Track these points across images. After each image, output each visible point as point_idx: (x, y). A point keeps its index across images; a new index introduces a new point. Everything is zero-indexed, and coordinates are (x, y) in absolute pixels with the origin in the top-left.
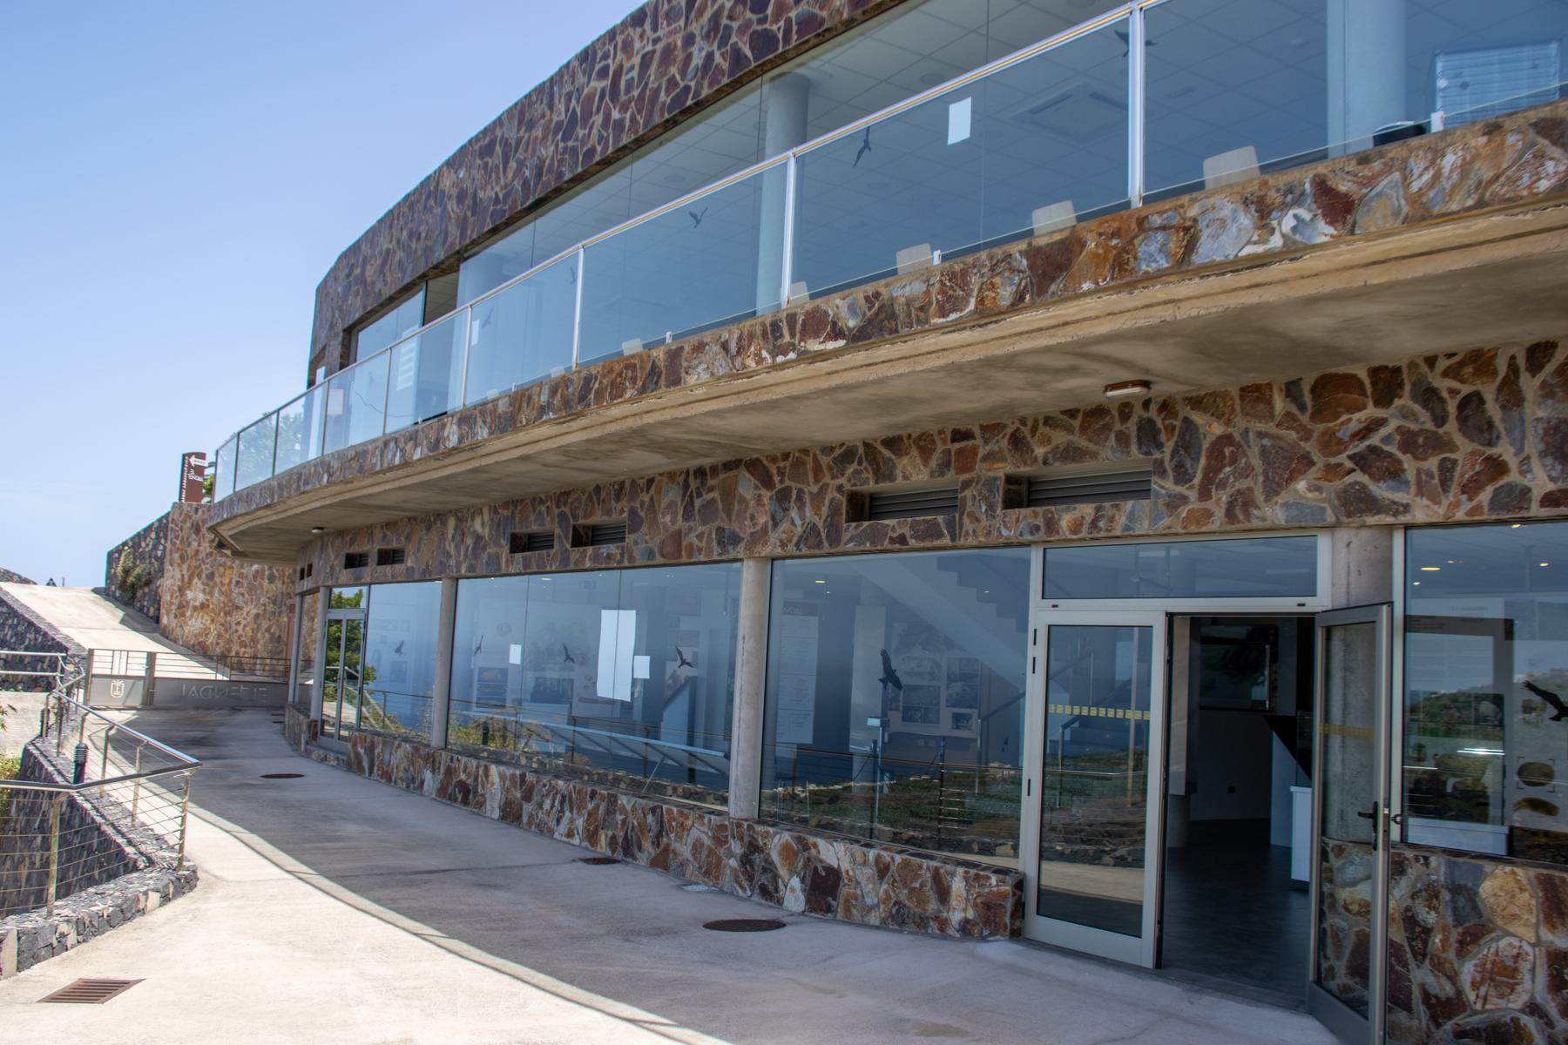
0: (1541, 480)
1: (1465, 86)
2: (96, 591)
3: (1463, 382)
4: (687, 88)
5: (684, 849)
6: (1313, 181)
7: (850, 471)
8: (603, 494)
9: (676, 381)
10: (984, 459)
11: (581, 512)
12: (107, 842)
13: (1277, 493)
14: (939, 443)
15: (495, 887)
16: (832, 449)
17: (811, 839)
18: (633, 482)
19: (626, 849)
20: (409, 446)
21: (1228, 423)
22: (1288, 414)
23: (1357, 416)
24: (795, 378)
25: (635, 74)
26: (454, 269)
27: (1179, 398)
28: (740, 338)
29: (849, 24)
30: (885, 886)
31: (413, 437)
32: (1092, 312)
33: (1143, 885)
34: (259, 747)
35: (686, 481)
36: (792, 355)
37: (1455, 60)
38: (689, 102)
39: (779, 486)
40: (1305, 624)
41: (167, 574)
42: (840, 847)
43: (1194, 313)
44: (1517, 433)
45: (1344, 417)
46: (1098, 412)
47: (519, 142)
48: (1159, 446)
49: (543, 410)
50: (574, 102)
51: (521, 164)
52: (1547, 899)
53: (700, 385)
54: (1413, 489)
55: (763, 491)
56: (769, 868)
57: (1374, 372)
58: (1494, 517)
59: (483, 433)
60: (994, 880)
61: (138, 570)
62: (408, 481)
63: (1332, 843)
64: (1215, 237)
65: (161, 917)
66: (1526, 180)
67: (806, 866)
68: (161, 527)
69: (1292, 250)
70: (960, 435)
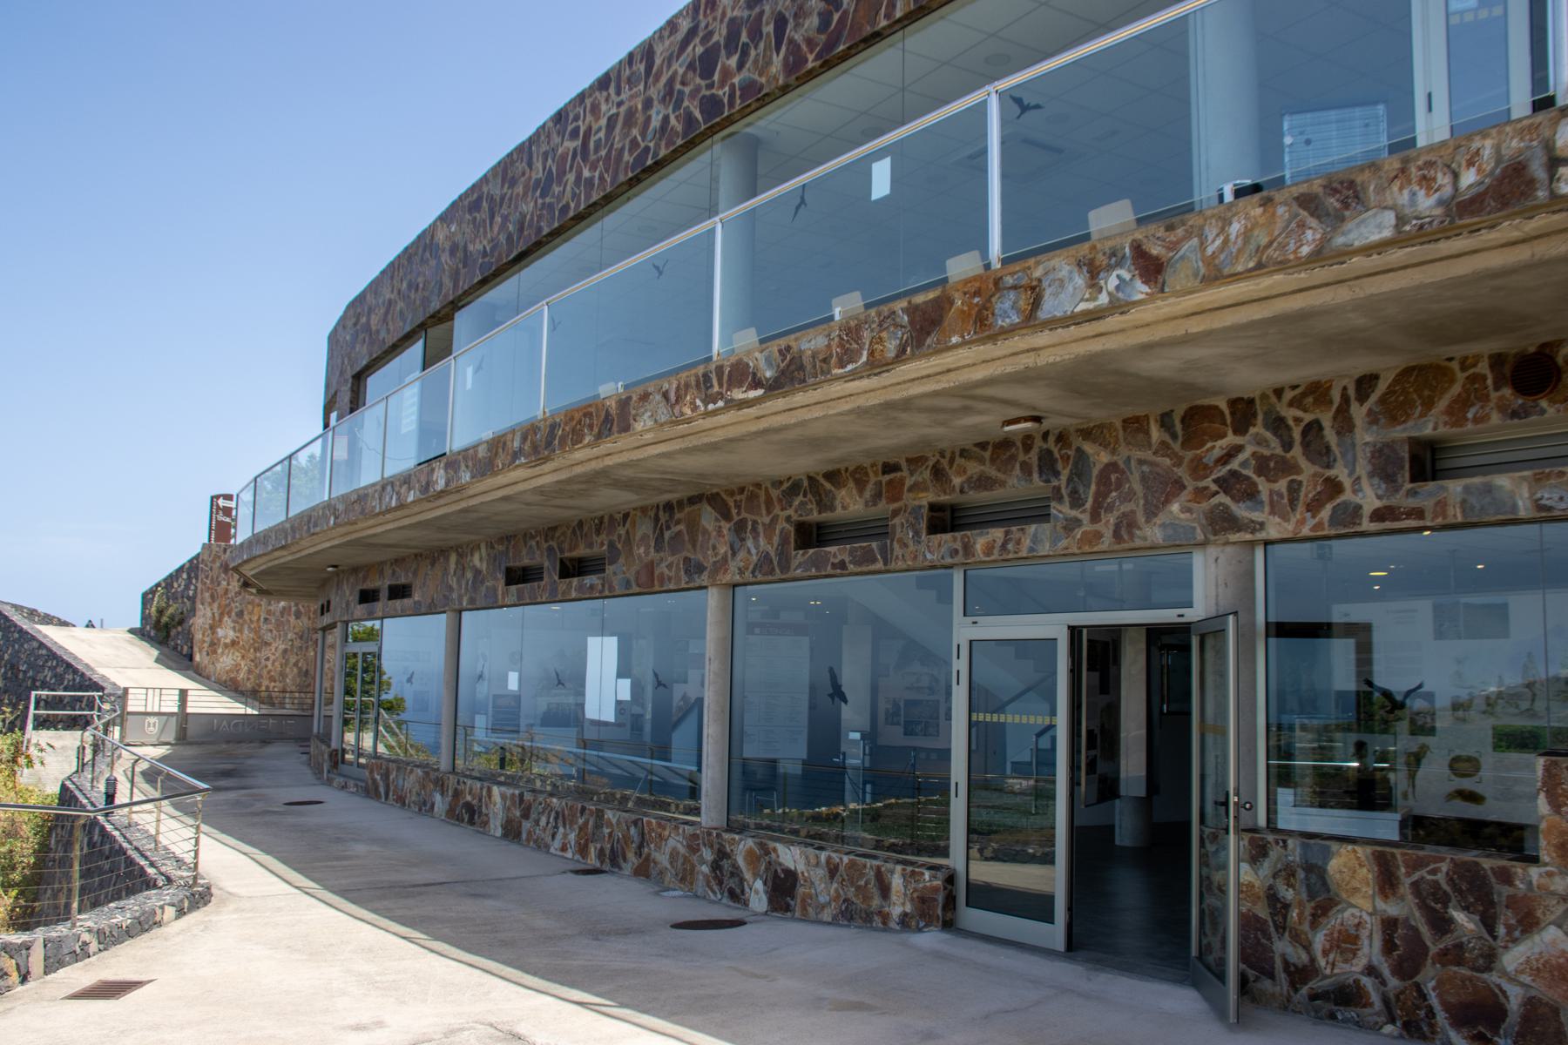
0: (1369, 498)
1: (1308, 142)
2: (132, 631)
3: (1305, 411)
4: (647, 149)
5: (663, 859)
6: (1131, 246)
7: (796, 503)
8: (586, 529)
9: (626, 428)
10: (910, 490)
11: (566, 546)
12: (130, 862)
13: (1156, 515)
14: (871, 474)
15: (484, 896)
16: (781, 483)
17: (771, 844)
18: (611, 517)
19: (613, 859)
20: (405, 487)
21: (1113, 452)
22: (1163, 443)
23: (1220, 443)
24: (728, 424)
25: (602, 134)
26: (449, 318)
27: (1072, 430)
28: (678, 388)
29: (785, 90)
30: (835, 885)
31: (406, 480)
32: (963, 362)
33: (1053, 879)
34: (286, 781)
35: (657, 515)
36: (720, 404)
37: (1299, 119)
38: (649, 162)
39: (736, 518)
40: (1184, 629)
41: (199, 613)
42: (796, 851)
43: (1051, 360)
44: (1349, 456)
45: (1209, 445)
46: (1005, 444)
47: (502, 198)
48: (1057, 474)
49: (515, 455)
50: (550, 161)
51: (505, 219)
52: (1381, 873)
53: (648, 431)
54: (1267, 509)
55: (723, 523)
56: (736, 873)
57: (1233, 403)
58: (1333, 532)
59: (466, 477)
60: (927, 876)
61: (171, 610)
62: (406, 522)
63: (1207, 831)
64: (1056, 295)
65: (176, 930)
66: (1292, 246)
67: (767, 869)
68: (192, 568)
69: (1118, 306)
70: (889, 468)
